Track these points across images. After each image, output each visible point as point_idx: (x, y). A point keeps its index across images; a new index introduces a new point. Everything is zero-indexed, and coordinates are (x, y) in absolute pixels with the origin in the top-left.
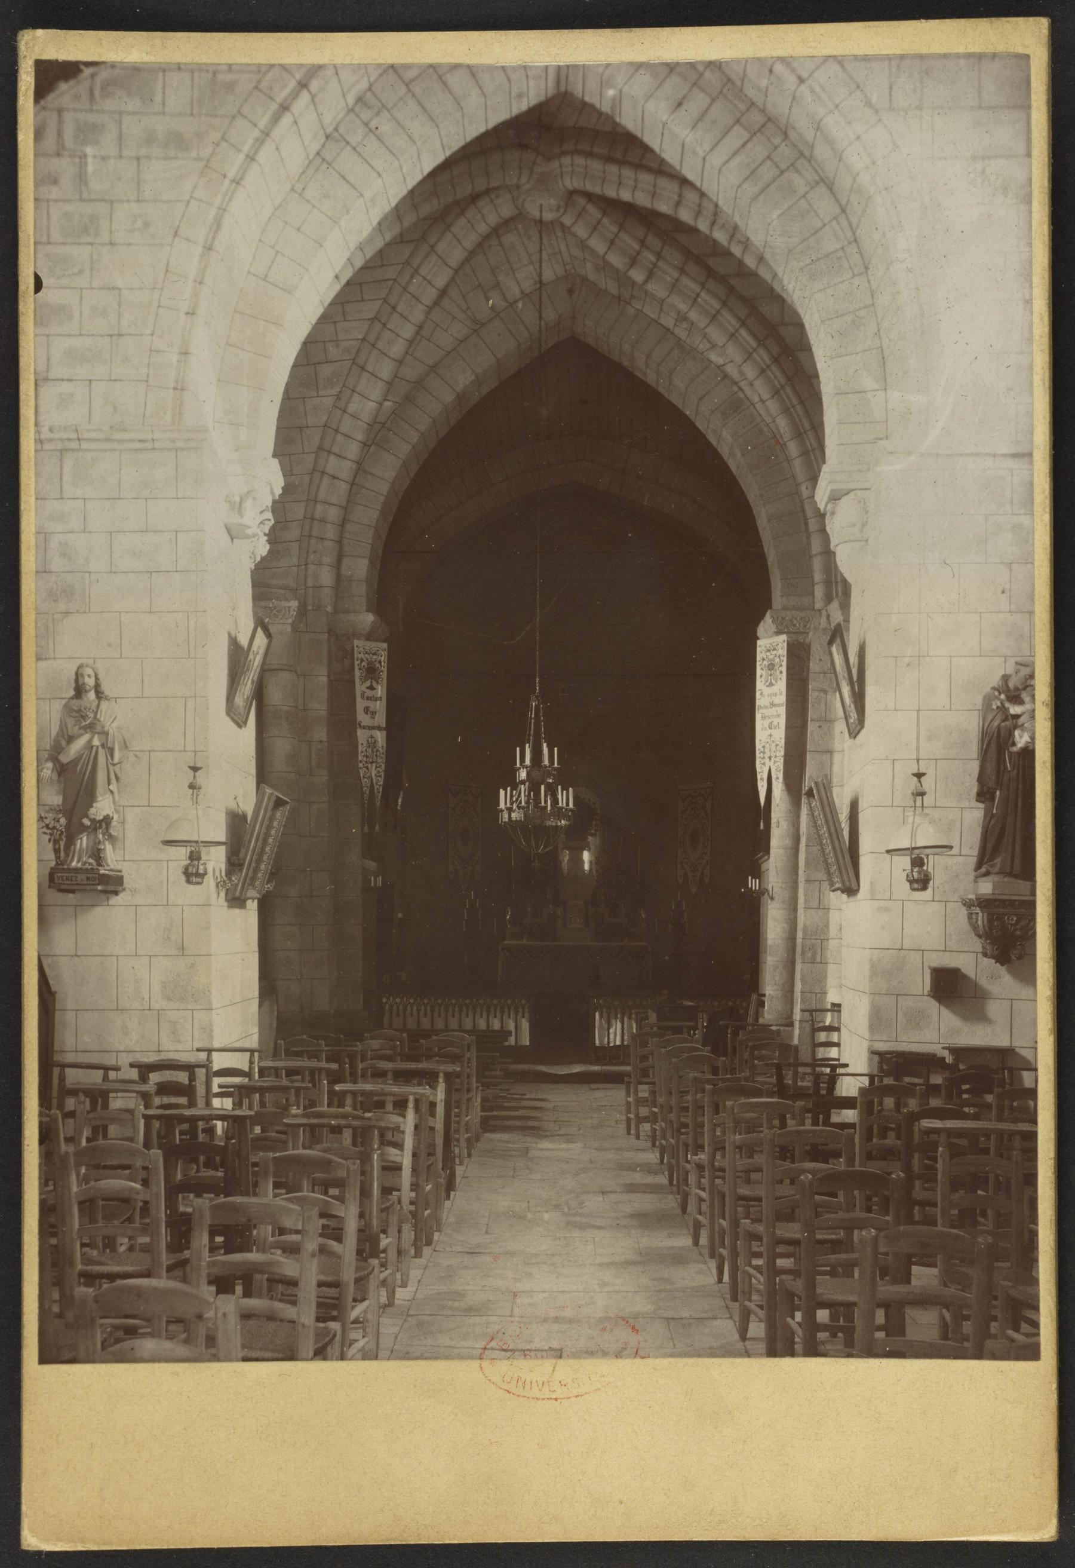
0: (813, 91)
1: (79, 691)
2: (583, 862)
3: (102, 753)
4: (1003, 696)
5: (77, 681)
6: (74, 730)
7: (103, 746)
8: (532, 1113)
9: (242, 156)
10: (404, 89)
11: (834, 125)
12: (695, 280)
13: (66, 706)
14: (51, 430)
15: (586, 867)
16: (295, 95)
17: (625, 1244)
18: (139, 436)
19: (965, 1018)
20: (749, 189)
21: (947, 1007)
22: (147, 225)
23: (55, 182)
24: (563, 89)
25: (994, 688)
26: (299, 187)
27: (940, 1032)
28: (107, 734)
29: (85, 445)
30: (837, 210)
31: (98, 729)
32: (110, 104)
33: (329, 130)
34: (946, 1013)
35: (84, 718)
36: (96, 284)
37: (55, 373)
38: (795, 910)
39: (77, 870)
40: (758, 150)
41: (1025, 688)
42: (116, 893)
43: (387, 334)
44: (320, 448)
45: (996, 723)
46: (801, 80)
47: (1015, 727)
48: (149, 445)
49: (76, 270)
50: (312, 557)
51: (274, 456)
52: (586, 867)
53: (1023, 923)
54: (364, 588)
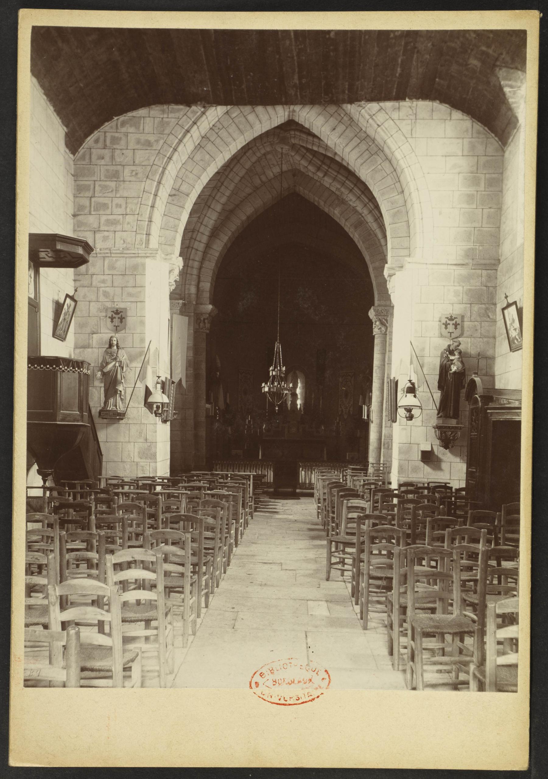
0: (383, 130)
1: (111, 346)
2: (297, 405)
3: (119, 368)
4: (448, 353)
5: (110, 342)
6: (109, 360)
7: (119, 366)
8: (274, 507)
9: (172, 149)
10: (231, 121)
11: (390, 142)
12: (343, 176)
13: (105, 351)
14: (100, 250)
15: (299, 407)
16: (192, 126)
17: (304, 543)
18: (134, 252)
19: (434, 469)
20: (360, 161)
21: (426, 464)
22: (137, 174)
23: (103, 158)
24: (291, 119)
25: (445, 350)
26: (191, 157)
27: (426, 475)
28: (121, 362)
29: (113, 255)
30: (393, 170)
31: (118, 360)
32: (124, 130)
33: (203, 135)
34: (426, 467)
35: (113, 356)
36: (118, 195)
37: (102, 228)
38: (382, 427)
39: (109, 411)
40: (363, 146)
41: (456, 350)
42: (122, 419)
43: (219, 194)
44: (191, 238)
45: (445, 362)
46: (379, 126)
47: (452, 364)
48: (137, 255)
49: (110, 190)
50: (187, 282)
51: (180, 256)
52: (299, 407)
53: (453, 434)
54: (208, 295)
